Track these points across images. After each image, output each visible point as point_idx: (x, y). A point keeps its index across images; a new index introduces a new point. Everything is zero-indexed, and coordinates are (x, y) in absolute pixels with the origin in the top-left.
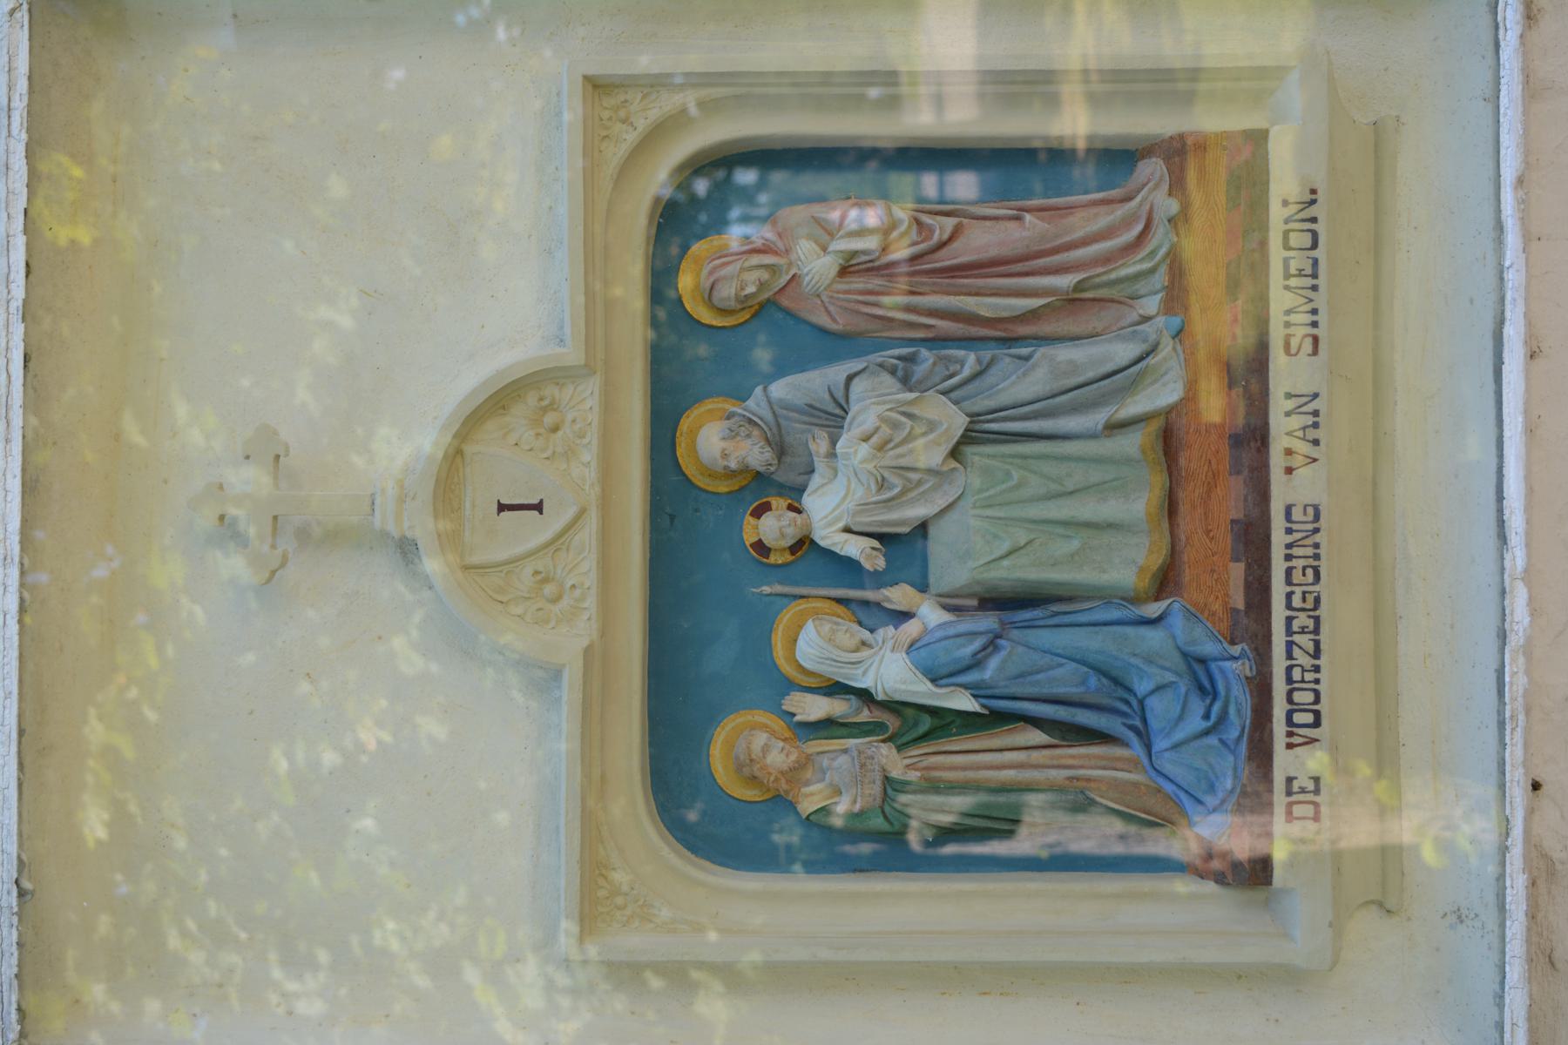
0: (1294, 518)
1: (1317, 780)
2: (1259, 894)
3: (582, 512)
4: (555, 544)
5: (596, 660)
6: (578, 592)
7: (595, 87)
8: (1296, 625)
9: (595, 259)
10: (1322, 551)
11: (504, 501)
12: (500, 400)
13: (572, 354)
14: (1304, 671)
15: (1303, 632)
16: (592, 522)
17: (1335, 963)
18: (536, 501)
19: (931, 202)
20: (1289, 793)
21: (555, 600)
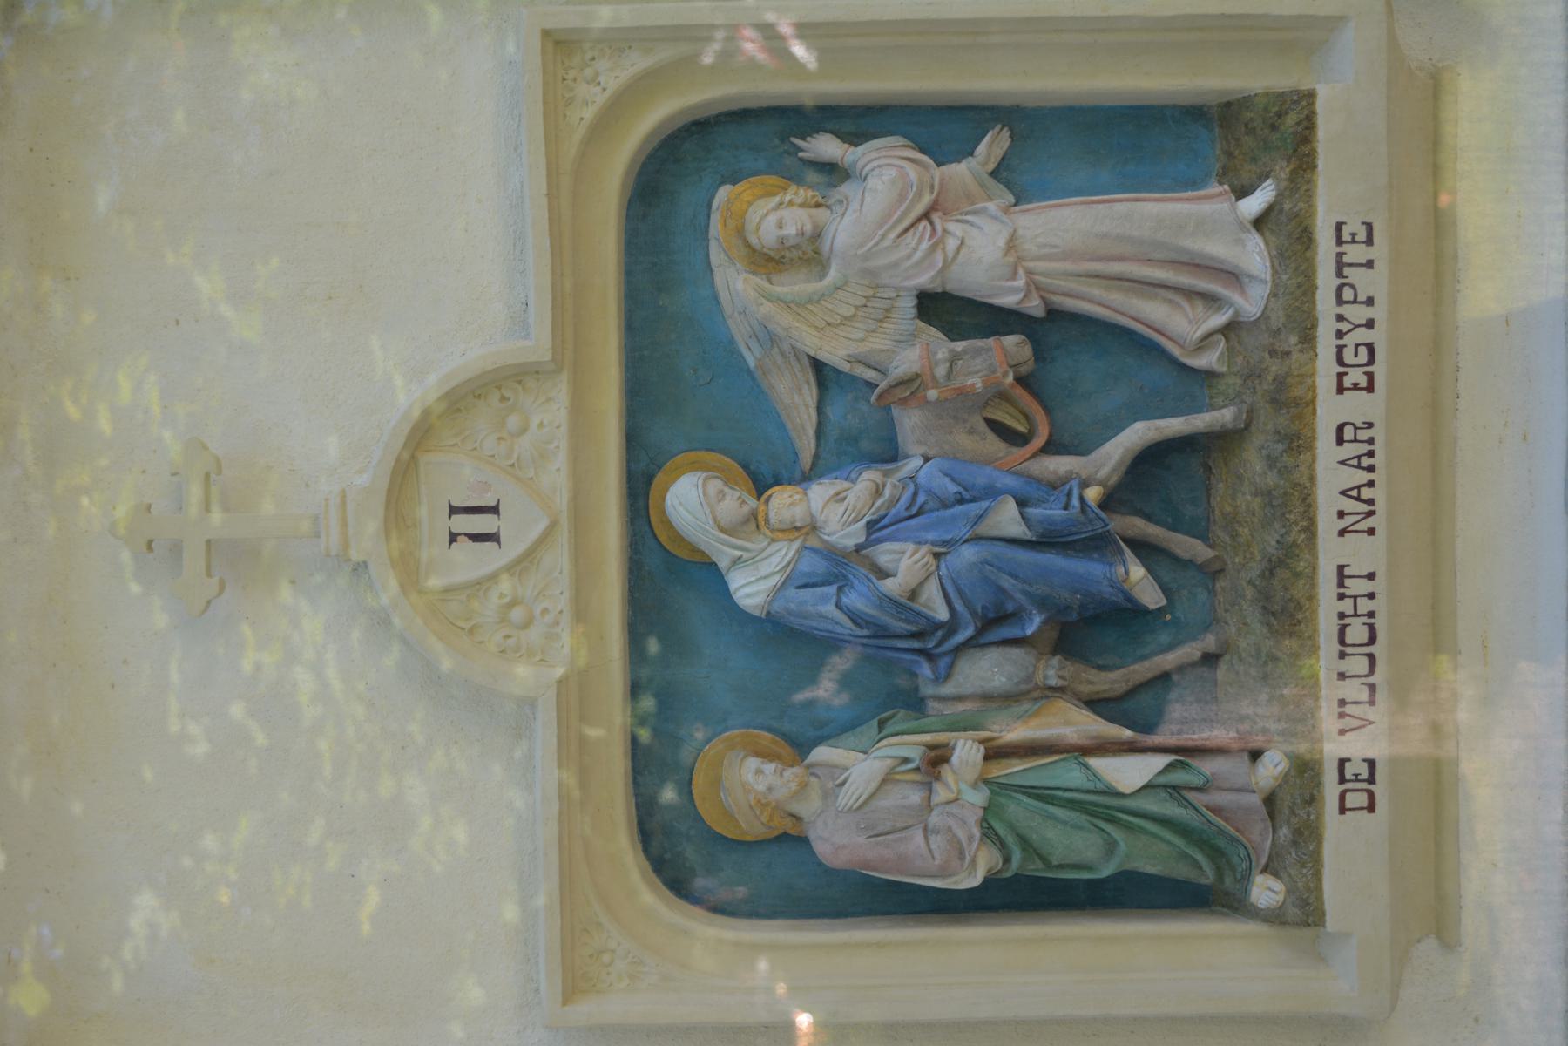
0: (1348, 640)
1: (1371, 764)
2: (1307, 933)
3: (553, 525)
4: (522, 565)
5: (573, 697)
6: (548, 618)
7: (557, 43)
8: (1347, 382)
9: (564, 244)
10: (1378, 447)
11: (455, 504)
12: (462, 399)
13: (538, 345)
14: (1356, 428)
15: (1354, 242)
16: (563, 535)
17: (1393, 1008)
18: (493, 503)
19: (1123, 795)
20: (1342, 780)
21: (526, 625)
